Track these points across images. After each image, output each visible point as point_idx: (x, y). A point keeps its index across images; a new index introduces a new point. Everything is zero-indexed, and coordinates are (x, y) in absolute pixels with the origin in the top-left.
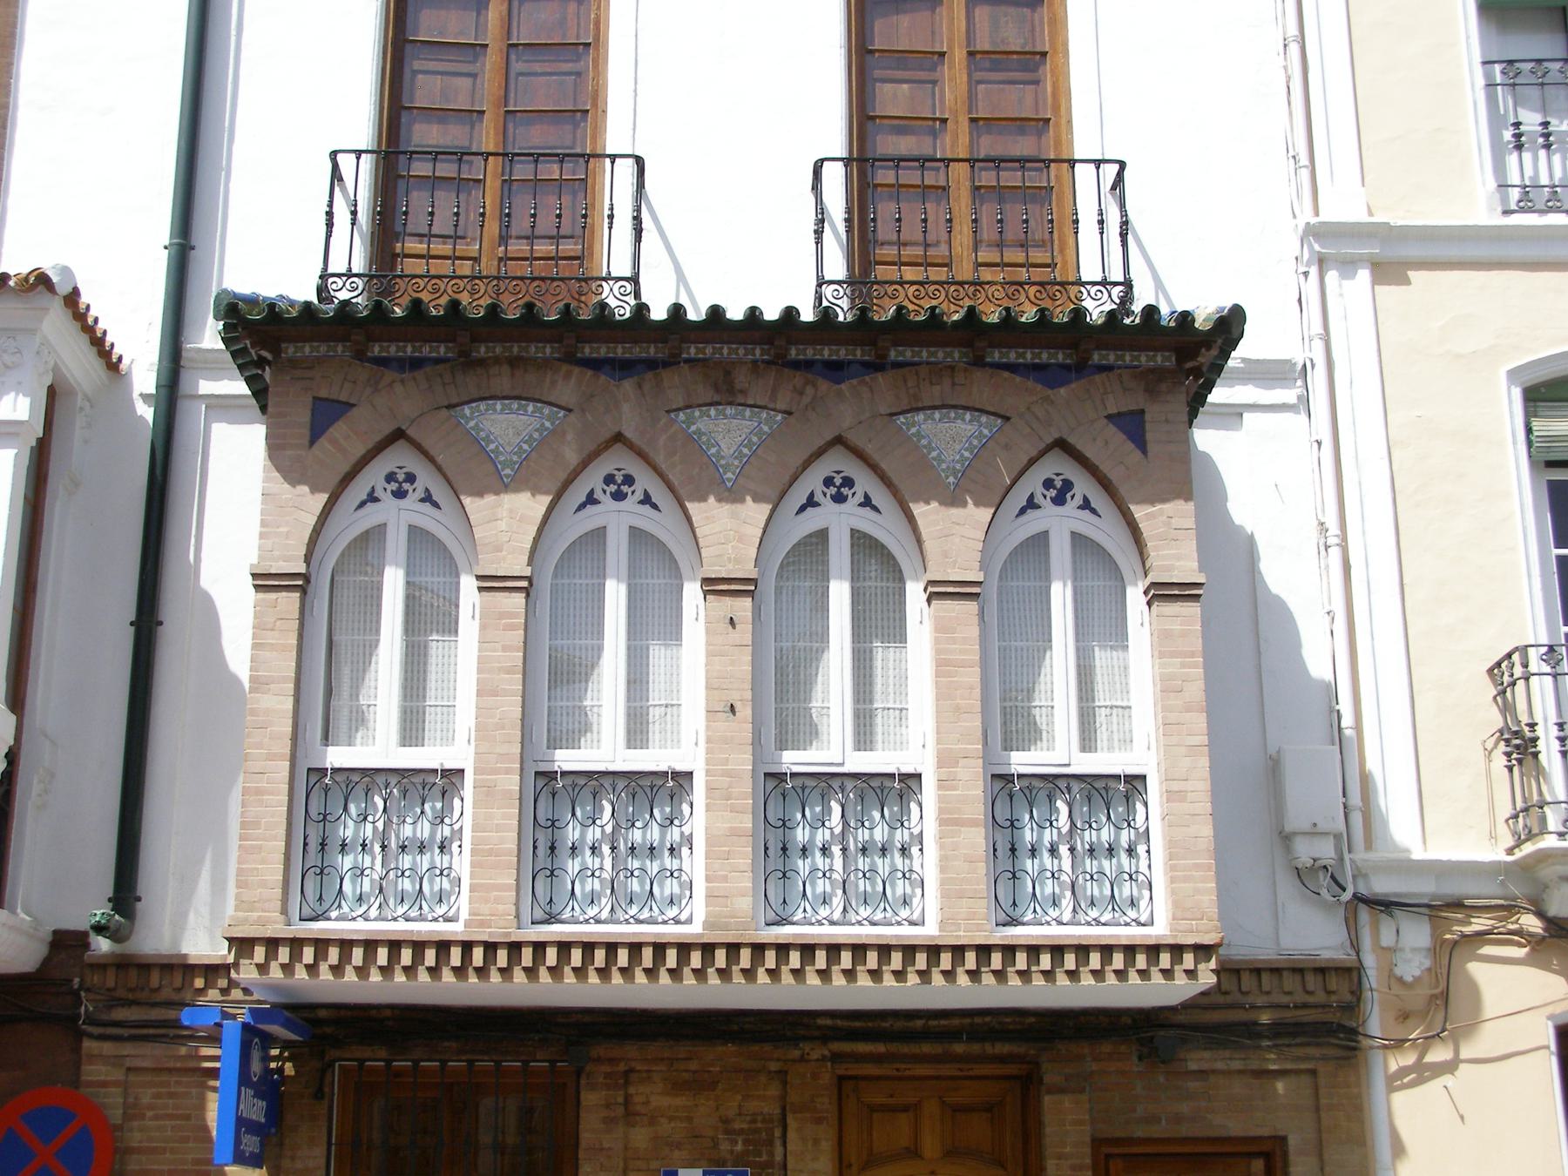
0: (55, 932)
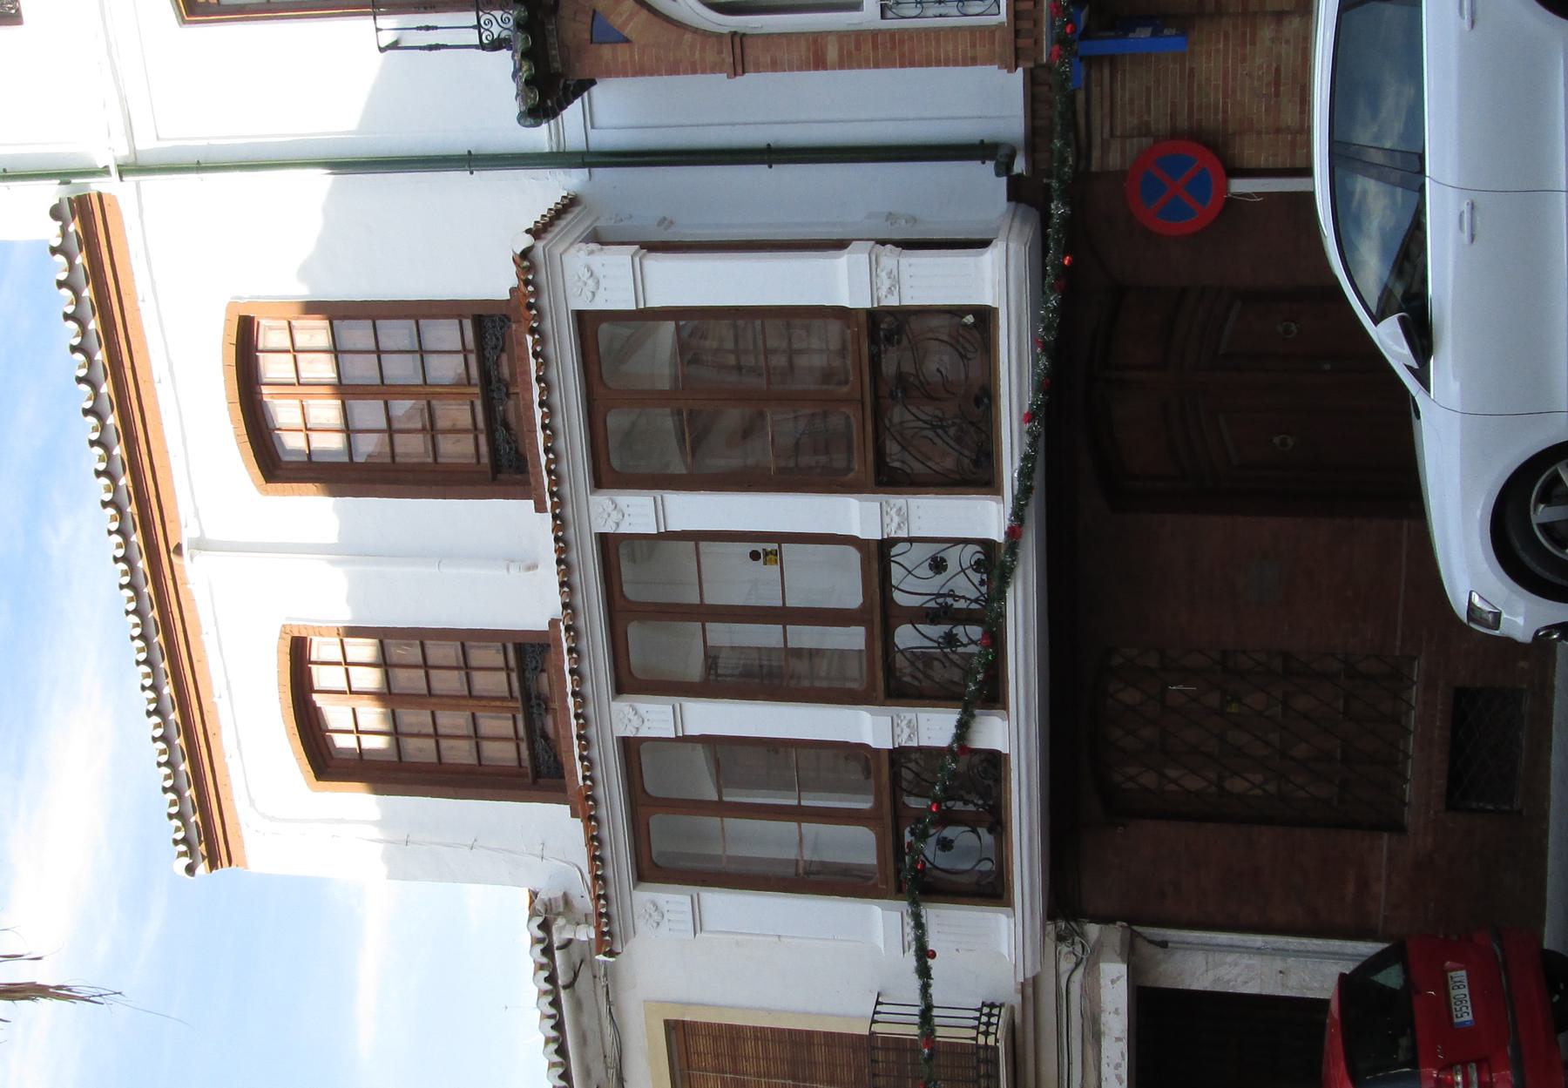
0: (1009, 199)
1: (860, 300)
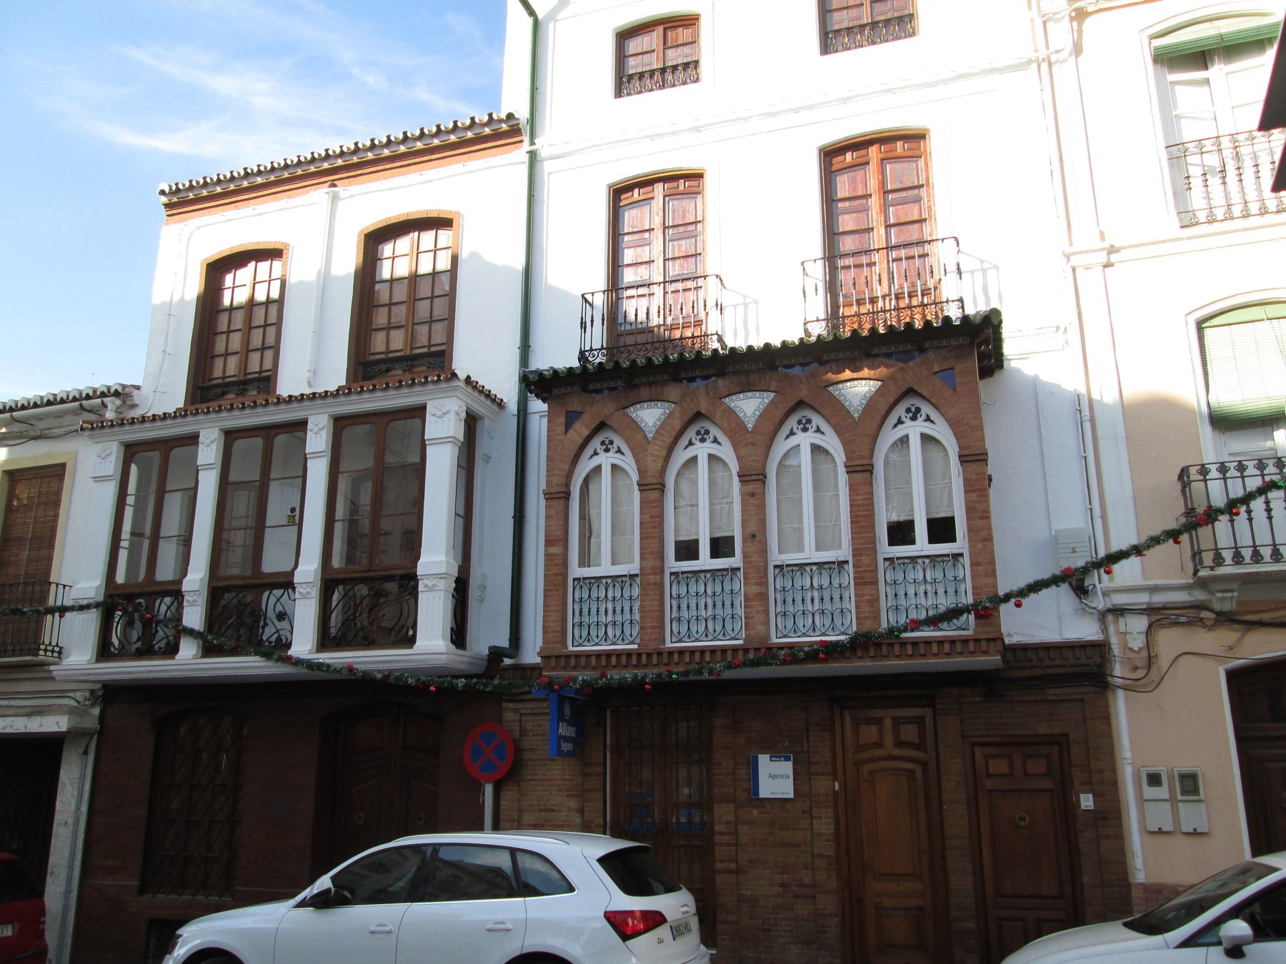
1: (422, 568)
